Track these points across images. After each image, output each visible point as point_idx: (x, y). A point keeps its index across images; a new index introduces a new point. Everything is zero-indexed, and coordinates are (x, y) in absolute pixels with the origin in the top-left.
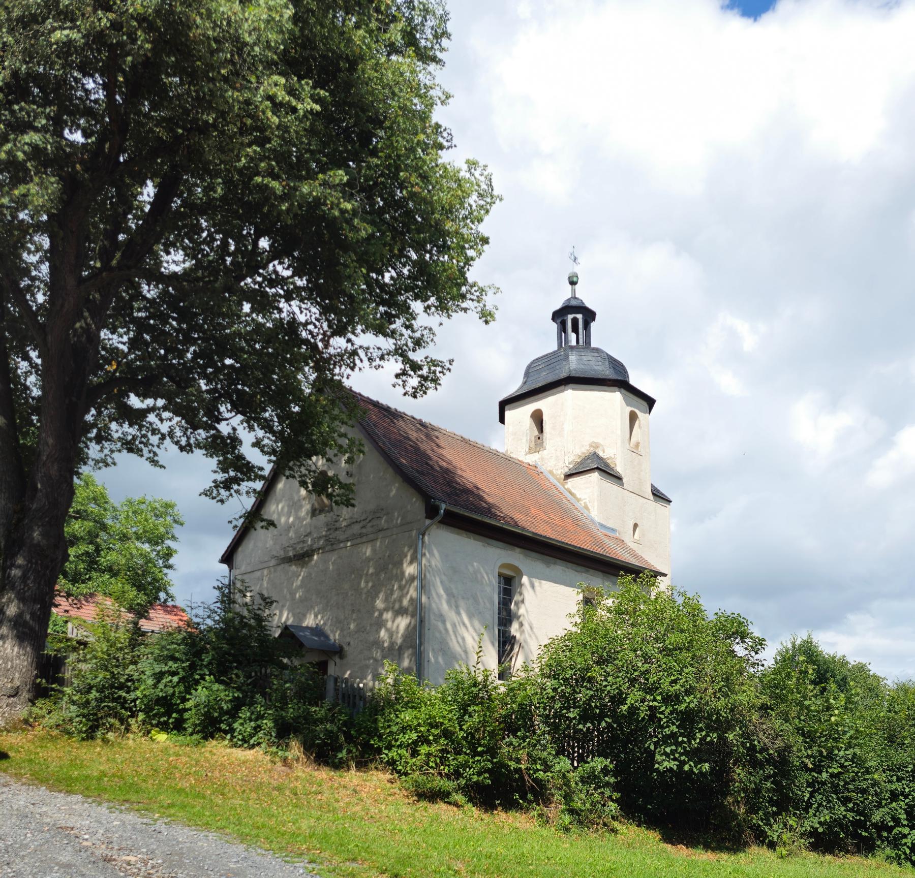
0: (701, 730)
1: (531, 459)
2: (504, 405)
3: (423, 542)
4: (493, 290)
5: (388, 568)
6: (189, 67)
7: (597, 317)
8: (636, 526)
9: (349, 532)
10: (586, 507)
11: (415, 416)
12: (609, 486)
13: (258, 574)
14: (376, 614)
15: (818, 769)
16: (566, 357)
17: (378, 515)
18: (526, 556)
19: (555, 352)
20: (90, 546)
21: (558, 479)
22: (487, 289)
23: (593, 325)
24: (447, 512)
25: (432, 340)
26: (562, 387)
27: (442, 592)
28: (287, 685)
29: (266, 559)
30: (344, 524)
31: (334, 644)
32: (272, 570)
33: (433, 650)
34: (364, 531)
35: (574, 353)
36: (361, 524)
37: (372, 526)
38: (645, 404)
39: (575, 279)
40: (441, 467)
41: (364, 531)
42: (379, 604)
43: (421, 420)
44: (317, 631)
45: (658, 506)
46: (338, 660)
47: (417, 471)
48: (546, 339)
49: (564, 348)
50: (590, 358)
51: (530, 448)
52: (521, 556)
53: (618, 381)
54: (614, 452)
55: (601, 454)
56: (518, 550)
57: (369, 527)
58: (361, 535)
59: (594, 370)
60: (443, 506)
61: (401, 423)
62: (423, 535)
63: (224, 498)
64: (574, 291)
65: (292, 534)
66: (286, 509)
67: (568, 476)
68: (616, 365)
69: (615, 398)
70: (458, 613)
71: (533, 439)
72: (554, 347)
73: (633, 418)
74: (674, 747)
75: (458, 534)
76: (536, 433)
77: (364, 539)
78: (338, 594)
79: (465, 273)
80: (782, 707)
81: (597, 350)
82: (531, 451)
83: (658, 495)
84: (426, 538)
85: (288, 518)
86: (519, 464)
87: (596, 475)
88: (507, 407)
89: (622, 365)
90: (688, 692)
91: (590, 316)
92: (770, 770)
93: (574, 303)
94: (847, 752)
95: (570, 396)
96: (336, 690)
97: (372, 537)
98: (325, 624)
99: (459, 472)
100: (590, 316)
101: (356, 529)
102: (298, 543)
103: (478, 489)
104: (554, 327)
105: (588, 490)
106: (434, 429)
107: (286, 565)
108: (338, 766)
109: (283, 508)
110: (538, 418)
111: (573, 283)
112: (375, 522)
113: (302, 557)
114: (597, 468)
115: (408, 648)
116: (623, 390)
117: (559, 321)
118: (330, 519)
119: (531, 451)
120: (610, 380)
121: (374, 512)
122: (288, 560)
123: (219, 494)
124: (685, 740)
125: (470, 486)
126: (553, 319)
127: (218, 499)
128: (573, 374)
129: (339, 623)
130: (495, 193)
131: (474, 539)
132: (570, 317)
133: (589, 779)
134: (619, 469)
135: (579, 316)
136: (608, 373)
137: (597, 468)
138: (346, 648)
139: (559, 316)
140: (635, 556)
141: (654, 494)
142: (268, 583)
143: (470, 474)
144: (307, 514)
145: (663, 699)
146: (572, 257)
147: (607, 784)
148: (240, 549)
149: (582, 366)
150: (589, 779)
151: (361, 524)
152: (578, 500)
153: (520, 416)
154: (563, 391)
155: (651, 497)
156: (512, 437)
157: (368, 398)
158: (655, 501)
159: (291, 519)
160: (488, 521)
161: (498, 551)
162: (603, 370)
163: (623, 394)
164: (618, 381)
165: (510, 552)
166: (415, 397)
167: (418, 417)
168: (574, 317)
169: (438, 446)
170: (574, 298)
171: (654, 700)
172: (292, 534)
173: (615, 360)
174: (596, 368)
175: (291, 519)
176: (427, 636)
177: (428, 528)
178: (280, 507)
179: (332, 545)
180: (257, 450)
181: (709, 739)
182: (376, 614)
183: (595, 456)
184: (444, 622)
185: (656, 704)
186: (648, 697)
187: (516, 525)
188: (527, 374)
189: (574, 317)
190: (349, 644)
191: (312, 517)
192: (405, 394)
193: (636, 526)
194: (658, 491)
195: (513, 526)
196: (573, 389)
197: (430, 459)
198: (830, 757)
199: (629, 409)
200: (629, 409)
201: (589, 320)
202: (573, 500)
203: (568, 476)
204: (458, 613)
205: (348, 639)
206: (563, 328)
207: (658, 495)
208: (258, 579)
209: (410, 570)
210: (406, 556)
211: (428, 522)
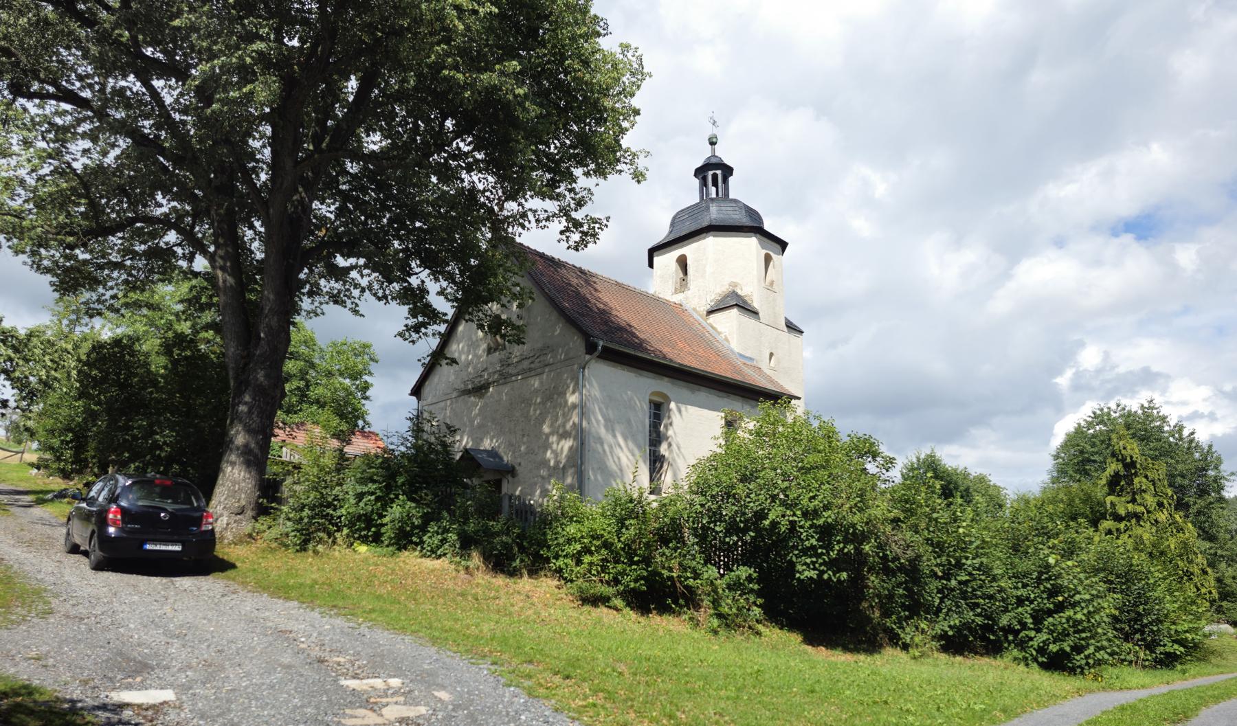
1: (677, 298)
2: (652, 252)
5: (554, 396)
8: (771, 355)
9: (520, 367)
10: (726, 339)
13: (442, 404)
16: (708, 208)
23: (731, 179)
27: (600, 418)
44: (493, 453)
45: (792, 337)
46: (510, 478)
48: (690, 194)
53: (754, 227)
54: (751, 290)
55: (740, 292)
57: (537, 363)
58: (530, 370)
60: (601, 343)
61: (564, 271)
64: (714, 150)
67: (710, 312)
69: (751, 243)
72: (696, 199)
73: (768, 259)
76: (681, 275)
82: (676, 291)
87: (735, 311)
91: (728, 171)
93: (714, 161)
95: (711, 243)
100: (728, 171)
101: (526, 364)
105: (728, 324)
106: (592, 275)
110: (683, 263)
111: (713, 143)
112: (542, 358)
113: (479, 390)
119: (676, 291)
122: (467, 392)
132: (710, 173)
133: (734, 586)
134: (756, 305)
135: (719, 172)
136: (746, 221)
139: (700, 172)
140: (772, 381)
143: (623, 313)
147: (752, 591)
152: (719, 333)
155: (785, 329)
156: (660, 280)
164: (754, 227)
168: (714, 172)
171: (794, 515)
183: (734, 294)
187: (665, 357)
188: (673, 224)
189: (714, 172)
193: (771, 355)
199: (764, 252)
200: (764, 252)
202: (715, 334)
203: (710, 312)
206: (704, 183)
209: (572, 399)
211: (588, 357)
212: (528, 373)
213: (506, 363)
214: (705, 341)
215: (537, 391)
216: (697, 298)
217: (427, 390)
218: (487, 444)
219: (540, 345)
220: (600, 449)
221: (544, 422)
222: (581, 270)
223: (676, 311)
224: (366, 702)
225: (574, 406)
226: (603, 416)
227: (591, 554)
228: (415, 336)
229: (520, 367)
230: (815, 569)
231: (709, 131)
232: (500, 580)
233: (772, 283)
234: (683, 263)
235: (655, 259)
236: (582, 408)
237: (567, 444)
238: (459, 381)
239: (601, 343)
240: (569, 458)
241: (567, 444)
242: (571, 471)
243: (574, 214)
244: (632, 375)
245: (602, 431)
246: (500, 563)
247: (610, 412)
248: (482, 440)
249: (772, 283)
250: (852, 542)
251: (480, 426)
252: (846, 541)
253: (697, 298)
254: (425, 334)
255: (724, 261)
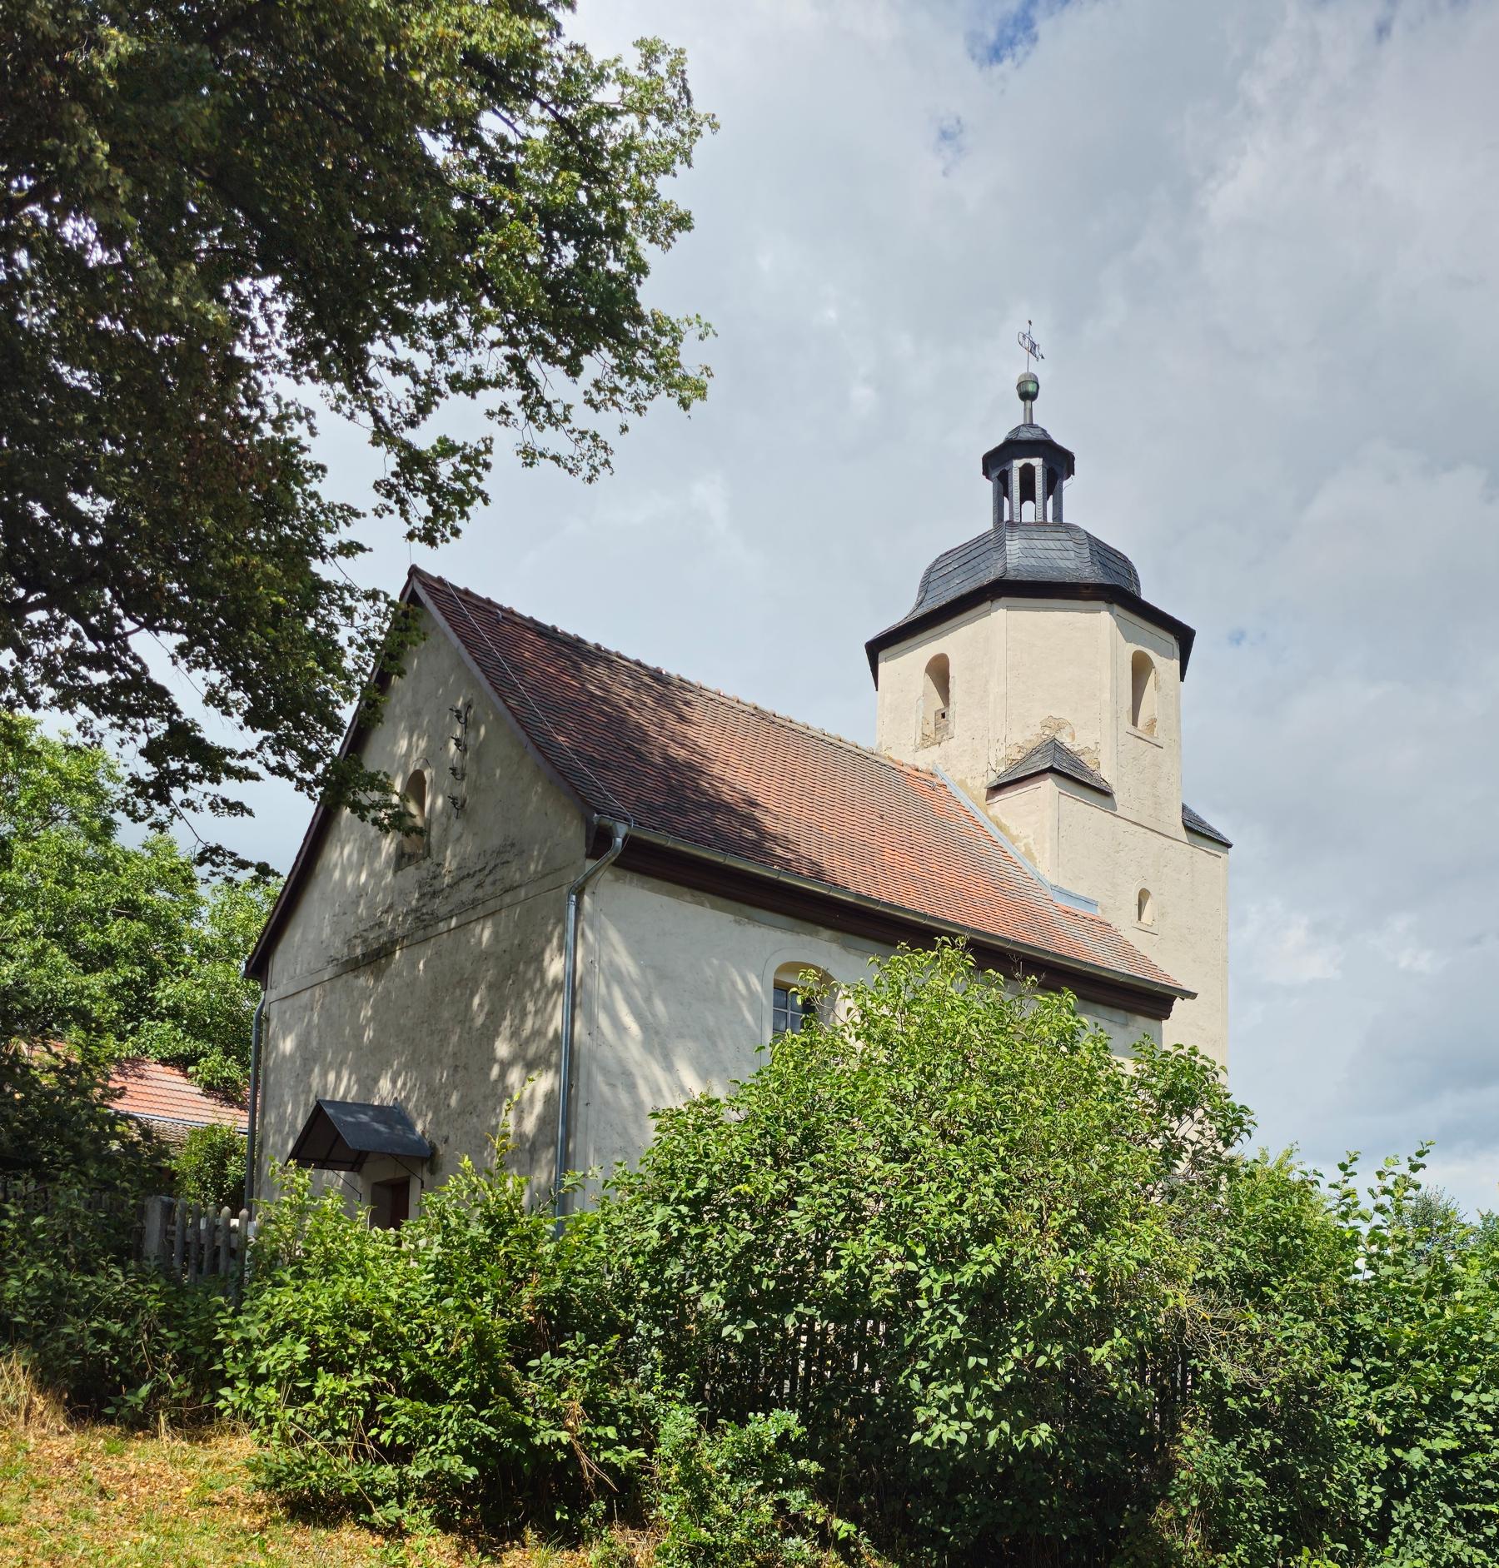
0: (1023, 1336)
1: (924, 759)
2: (877, 648)
3: (578, 909)
4: (697, 331)
5: (515, 971)
6: (595, 204)
7: (1078, 465)
8: (1143, 896)
9: (456, 898)
10: (1029, 854)
11: (644, 661)
12: (1080, 810)
13: (306, 995)
14: (495, 1071)
15: (1404, 1436)
16: (1001, 544)
17: (506, 857)
18: (845, 946)
19: (981, 540)
20: (138, 969)
21: (974, 798)
22: (684, 327)
23: (1069, 486)
24: (631, 842)
25: (607, 462)
26: (986, 605)
27: (628, 1020)
28: (38, 1221)
29: (319, 966)
30: (447, 880)
31: (420, 1141)
32: (328, 985)
33: (598, 1150)
34: (480, 893)
35: (1017, 535)
36: (475, 881)
37: (494, 883)
38: (1171, 638)
39: (1031, 388)
40: (667, 758)
41: (480, 893)
42: (503, 1049)
43: (658, 671)
44: (394, 1116)
45: (1203, 857)
46: (426, 1177)
47: (591, 761)
48: (971, 510)
49: (1004, 525)
50: (1051, 544)
51: (925, 737)
52: (835, 948)
53: (1112, 587)
54: (1097, 740)
55: (1068, 743)
56: (827, 934)
57: (488, 886)
58: (474, 903)
59: (1059, 569)
60: (622, 830)
61: (601, 671)
62: (580, 893)
63: (164, 819)
64: (1030, 412)
65: (362, 910)
66: (355, 857)
67: (996, 789)
68: (1103, 553)
69: (1099, 626)
70: (669, 1068)
71: (932, 719)
72: (986, 524)
73: (1141, 669)
74: (958, 1388)
75: (669, 894)
76: (939, 704)
77: (480, 911)
78: (432, 1033)
79: (634, 292)
80: (1296, 1281)
81: (1070, 528)
82: (927, 741)
83: (1196, 830)
84: (586, 899)
85: (359, 876)
86: (893, 769)
87: (1049, 785)
88: (881, 655)
89: (1125, 560)
90: (984, 1236)
91: (1060, 463)
92: (1265, 1439)
93: (1025, 435)
94: (1485, 1398)
95: (1001, 622)
96: (166, 1233)
97: (492, 905)
98: (407, 1098)
99: (716, 770)
100: (1060, 463)
101: (467, 890)
102: (372, 928)
103: (753, 804)
104: (988, 487)
105: (1035, 821)
106: (684, 685)
107: (351, 976)
108: (139, 1424)
109: (350, 855)
110: (939, 672)
111: (1027, 396)
112: (498, 875)
113: (374, 959)
114: (1051, 770)
115: (548, 1146)
116: (1117, 609)
117: (995, 474)
118: (424, 874)
119: (927, 741)
120: (1087, 586)
121: (499, 853)
122: (353, 966)
123: (151, 811)
124: (984, 1362)
125: (727, 795)
126: (986, 473)
127: (151, 820)
128: (1011, 576)
129: (434, 1096)
130: (700, 107)
131: (713, 907)
132: (1018, 463)
133: (758, 1465)
134: (1107, 773)
135: (1037, 462)
136: (1090, 573)
137: (1051, 770)
138: (442, 1149)
139: (995, 462)
140: (1128, 951)
141: (1188, 829)
142: (320, 1016)
143: (735, 771)
144: (387, 863)
145: (931, 1252)
146: (1027, 343)
147: (801, 1479)
148: (281, 947)
149: (1033, 562)
150: (758, 1465)
151: (475, 881)
152: (1014, 840)
153: (907, 667)
154: (987, 613)
155: (1183, 835)
156: (883, 715)
157: (531, 620)
158: (1192, 844)
159: (363, 878)
160: (742, 865)
161: (778, 935)
162: (1072, 564)
163: (1117, 617)
164: (1112, 587)
165: (806, 938)
166: (432, 542)
167: (651, 663)
168: (1030, 463)
169: (682, 718)
170: (1031, 425)
171: (911, 1256)
172: (362, 910)
173: (1107, 549)
174: (1062, 564)
175: (363, 878)
176: (581, 1119)
177: (588, 878)
178: (346, 851)
179: (425, 928)
180: (214, 712)
181: (1042, 1361)
182: (495, 1071)
183: (1055, 746)
184: (632, 1087)
185: (912, 1266)
186: (892, 1249)
187: (818, 875)
188: (926, 585)
189: (1030, 463)
190: (446, 1141)
191: (395, 872)
192: (411, 536)
193: (1143, 896)
194: (1201, 823)
195: (805, 879)
196: (1008, 608)
197: (644, 738)
198: (1442, 1408)
199: (1133, 648)
200: (1133, 648)
201: (1057, 469)
202: (1005, 844)
203: (996, 789)
204: (669, 1068)
205: (445, 1131)
206: (1003, 490)
207: (1196, 830)
208: (305, 1008)
209: (555, 967)
210: (549, 941)
211: (590, 864)
212: (472, 911)
213: (430, 892)
214: (979, 854)
215: (485, 956)
216: (966, 762)
217: (280, 964)
218: (386, 1090)
219: (495, 841)
220: (625, 1099)
221: (497, 1034)
222: (657, 675)
223: (920, 788)
224: (1484, 1416)
225: (558, 985)
226: (639, 1016)
227: (340, 1369)
228: (162, 812)
229: (456, 898)
230: (961, 1416)
231: (1017, 367)
232: (99, 1439)
233: (1152, 724)
234: (939, 672)
235: (882, 666)
236: (573, 990)
237: (545, 1083)
238: (338, 942)
239: (622, 830)
240: (544, 1122)
241: (545, 1083)
242: (548, 1155)
243: (408, 435)
244: (725, 918)
245: (633, 1049)
246: (93, 1395)
247: (659, 1007)
248: (376, 1081)
249: (1152, 724)
250: (1061, 1335)
251: (377, 1047)
252: (1046, 1332)
253: (966, 762)
254: (188, 804)
255: (1041, 668)
